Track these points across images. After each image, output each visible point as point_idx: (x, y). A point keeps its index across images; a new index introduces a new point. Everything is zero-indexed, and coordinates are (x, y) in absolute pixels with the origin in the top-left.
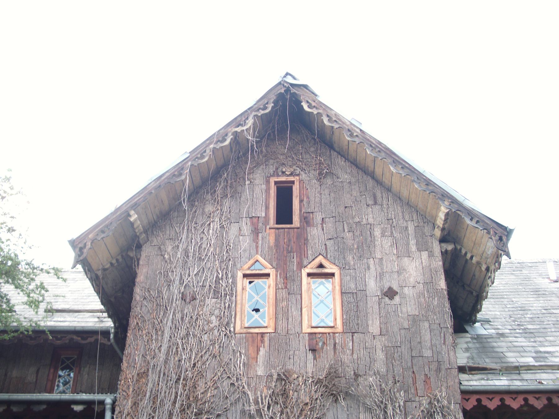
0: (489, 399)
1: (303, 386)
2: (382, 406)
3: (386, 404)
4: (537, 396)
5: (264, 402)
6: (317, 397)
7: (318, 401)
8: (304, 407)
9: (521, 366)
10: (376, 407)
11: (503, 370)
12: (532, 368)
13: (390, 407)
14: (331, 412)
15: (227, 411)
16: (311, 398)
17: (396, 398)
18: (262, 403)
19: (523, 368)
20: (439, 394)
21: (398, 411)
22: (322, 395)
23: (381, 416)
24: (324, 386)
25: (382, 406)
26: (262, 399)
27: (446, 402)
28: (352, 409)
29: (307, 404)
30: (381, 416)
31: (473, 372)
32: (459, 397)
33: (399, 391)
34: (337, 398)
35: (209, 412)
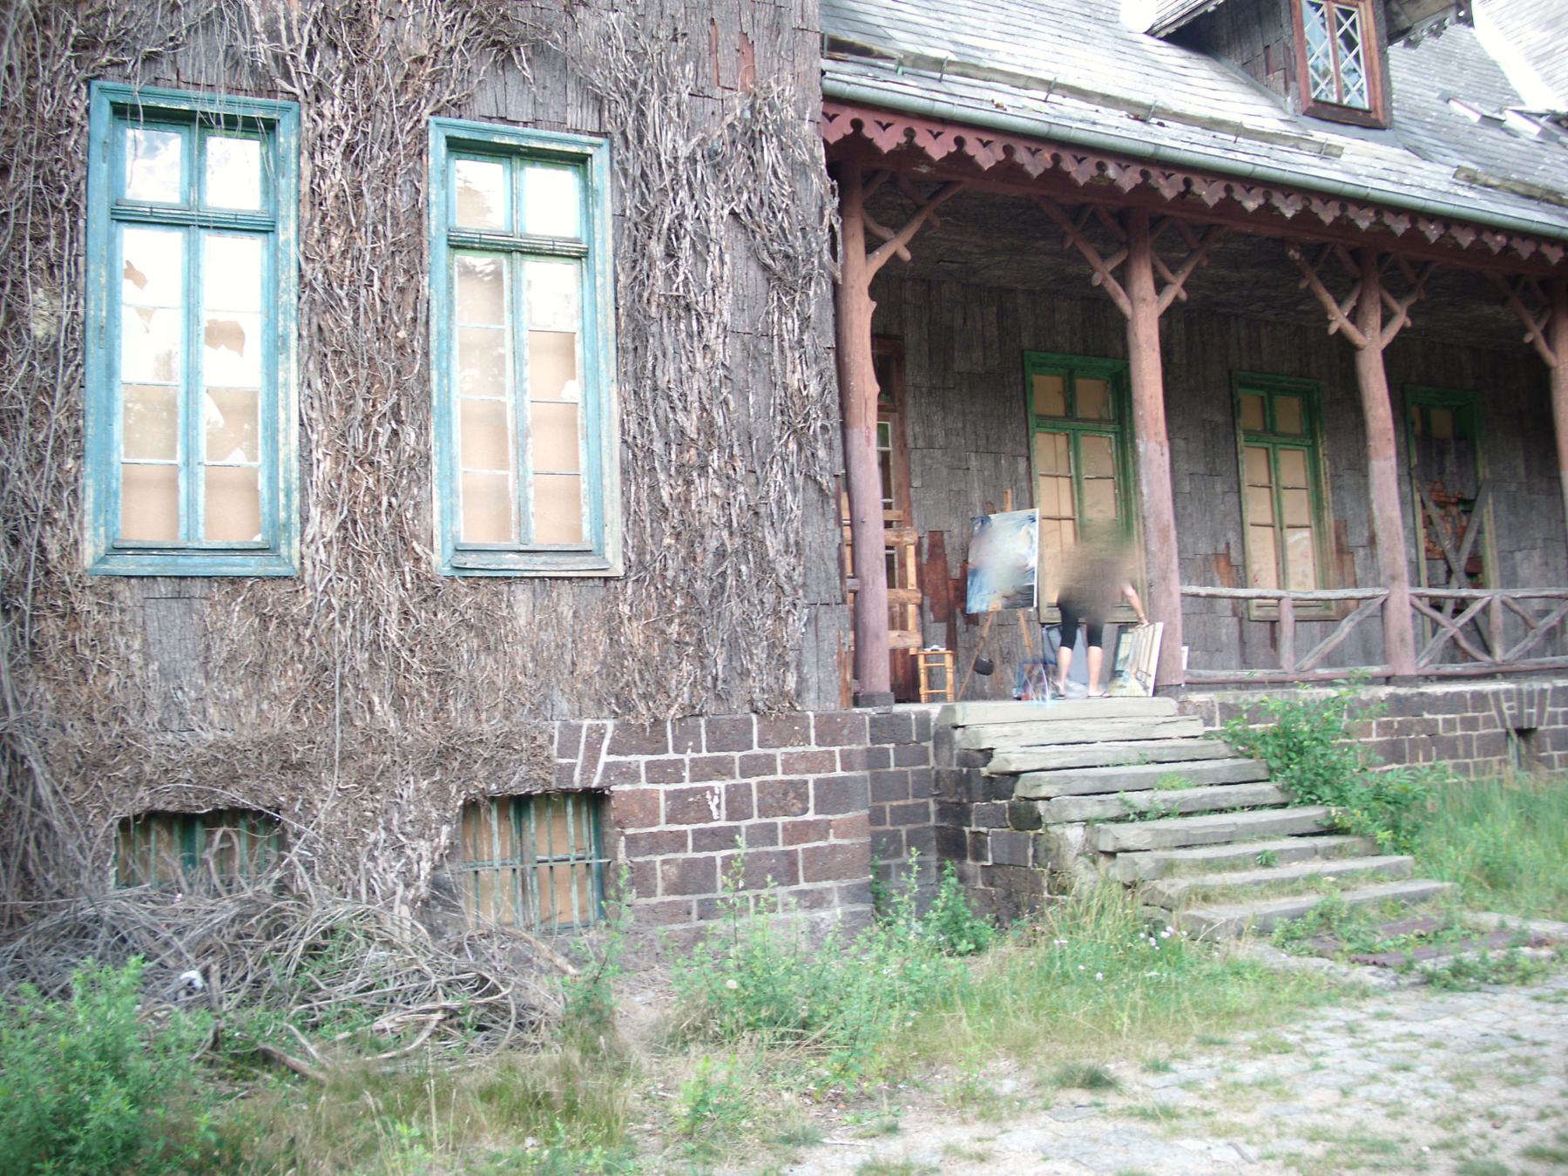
0: (880, 123)
1: (411, 7)
2: (635, 96)
3: (644, 91)
4: (986, 138)
5: (296, 34)
6: (452, 43)
7: (456, 56)
8: (413, 67)
9: (951, 63)
10: (617, 96)
11: (907, 62)
12: (972, 72)
13: (654, 100)
14: (490, 93)
15: (177, 47)
16: (435, 44)
17: (673, 81)
18: (291, 40)
19: (951, 69)
20: (776, 89)
21: (674, 114)
22: (466, 41)
23: (630, 121)
24: (473, 16)
25: (635, 96)
26: (289, 28)
27: (790, 113)
28: (548, 92)
29: (422, 60)
30: (630, 121)
31: (838, 55)
32: (816, 106)
33: (682, 62)
34: (510, 56)
35: (116, 44)
